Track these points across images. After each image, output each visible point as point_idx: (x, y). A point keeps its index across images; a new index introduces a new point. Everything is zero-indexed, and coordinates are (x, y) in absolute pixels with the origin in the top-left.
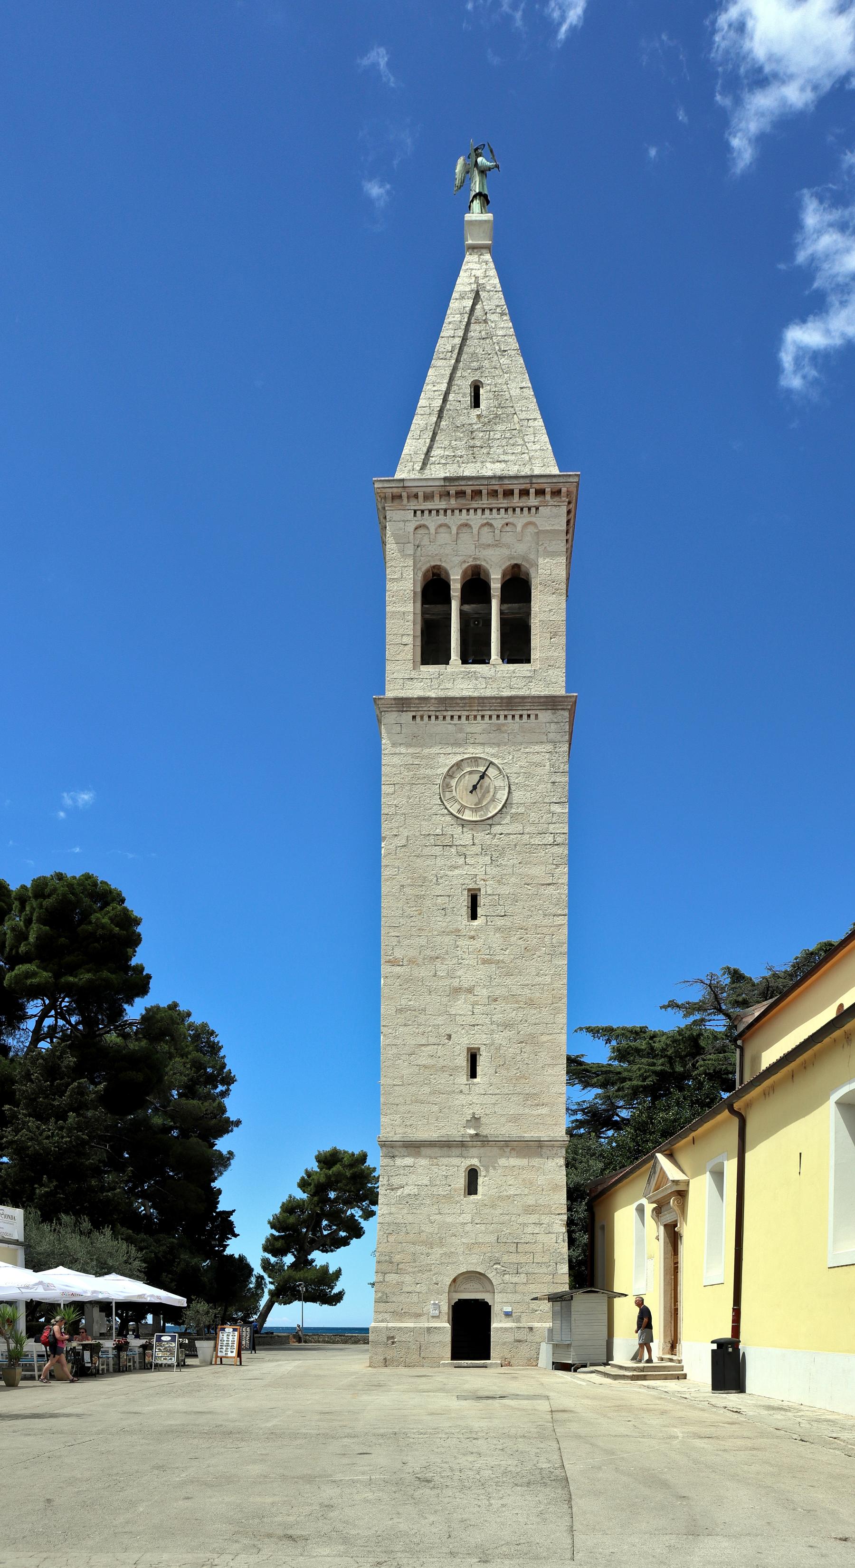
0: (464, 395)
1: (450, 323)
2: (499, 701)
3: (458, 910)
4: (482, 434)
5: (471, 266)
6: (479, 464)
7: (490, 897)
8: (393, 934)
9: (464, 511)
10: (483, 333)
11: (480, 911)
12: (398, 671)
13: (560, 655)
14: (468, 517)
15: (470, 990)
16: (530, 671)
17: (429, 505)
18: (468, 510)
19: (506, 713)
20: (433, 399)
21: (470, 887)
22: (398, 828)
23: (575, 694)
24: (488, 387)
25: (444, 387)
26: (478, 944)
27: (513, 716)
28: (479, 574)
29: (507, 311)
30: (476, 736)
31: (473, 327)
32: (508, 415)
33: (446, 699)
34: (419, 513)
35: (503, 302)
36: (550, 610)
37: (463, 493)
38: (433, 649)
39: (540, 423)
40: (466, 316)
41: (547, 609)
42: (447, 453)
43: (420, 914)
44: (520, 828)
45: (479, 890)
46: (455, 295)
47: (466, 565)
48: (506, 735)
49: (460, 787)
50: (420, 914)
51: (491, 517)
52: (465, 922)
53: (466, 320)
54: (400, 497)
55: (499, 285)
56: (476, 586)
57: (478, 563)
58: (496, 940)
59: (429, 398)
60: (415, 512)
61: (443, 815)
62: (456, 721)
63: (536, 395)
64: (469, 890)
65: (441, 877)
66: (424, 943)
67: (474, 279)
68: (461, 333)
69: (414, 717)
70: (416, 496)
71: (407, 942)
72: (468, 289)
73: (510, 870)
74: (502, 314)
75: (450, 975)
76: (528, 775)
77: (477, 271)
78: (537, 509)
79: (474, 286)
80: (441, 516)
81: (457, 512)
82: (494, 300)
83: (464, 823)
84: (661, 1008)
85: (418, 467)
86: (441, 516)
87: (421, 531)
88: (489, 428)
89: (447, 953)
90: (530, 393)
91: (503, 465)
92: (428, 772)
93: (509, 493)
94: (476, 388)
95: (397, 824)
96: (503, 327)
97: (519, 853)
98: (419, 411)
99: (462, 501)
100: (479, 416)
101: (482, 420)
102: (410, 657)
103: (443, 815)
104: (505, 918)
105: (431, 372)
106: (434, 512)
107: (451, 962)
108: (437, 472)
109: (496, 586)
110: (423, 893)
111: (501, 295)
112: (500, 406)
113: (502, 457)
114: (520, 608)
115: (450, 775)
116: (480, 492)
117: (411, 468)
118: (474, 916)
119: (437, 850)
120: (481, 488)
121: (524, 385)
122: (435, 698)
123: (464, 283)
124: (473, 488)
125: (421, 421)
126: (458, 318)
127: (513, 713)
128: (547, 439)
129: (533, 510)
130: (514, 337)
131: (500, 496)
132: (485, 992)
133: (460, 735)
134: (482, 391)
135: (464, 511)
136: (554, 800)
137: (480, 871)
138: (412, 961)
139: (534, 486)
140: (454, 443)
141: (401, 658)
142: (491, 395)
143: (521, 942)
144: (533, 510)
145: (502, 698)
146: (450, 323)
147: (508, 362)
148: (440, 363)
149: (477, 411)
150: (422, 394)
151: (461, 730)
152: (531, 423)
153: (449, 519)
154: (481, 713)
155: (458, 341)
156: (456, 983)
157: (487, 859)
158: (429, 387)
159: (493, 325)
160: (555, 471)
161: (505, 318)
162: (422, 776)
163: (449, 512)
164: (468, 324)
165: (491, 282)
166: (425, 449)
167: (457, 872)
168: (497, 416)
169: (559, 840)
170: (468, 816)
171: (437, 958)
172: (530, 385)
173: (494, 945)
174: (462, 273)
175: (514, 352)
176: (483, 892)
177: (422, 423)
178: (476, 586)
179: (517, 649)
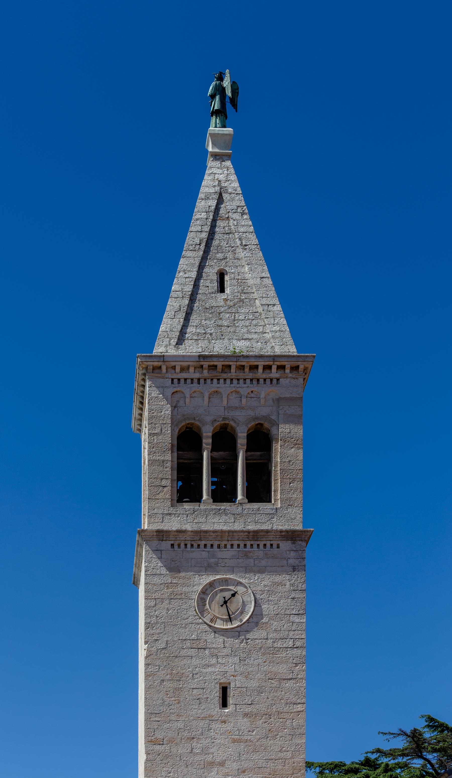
0: (212, 281)
1: (197, 220)
2: (246, 534)
3: (211, 700)
4: (228, 315)
5: (214, 170)
6: (226, 341)
7: (239, 690)
8: (154, 719)
9: (215, 381)
10: (227, 228)
11: (230, 701)
12: (158, 508)
13: (298, 496)
14: (218, 385)
15: (222, 764)
16: (272, 509)
17: (185, 375)
18: (218, 380)
19: (252, 542)
20: (185, 284)
21: (222, 681)
22: (159, 634)
23: (312, 529)
24: (233, 275)
25: (194, 275)
26: (229, 727)
27: (258, 545)
28: (226, 428)
29: (247, 211)
30: (226, 561)
31: (219, 223)
32: (250, 300)
33: (201, 532)
34: (176, 381)
35: (243, 203)
36: (290, 461)
37: (215, 368)
38: (187, 491)
39: (278, 308)
40: (211, 215)
41: (286, 456)
42: (198, 331)
43: (178, 703)
44: (264, 634)
45: (230, 683)
46: (201, 195)
47: (218, 423)
48: (252, 561)
49: (213, 607)
50: (178, 703)
51: (238, 386)
52: (217, 709)
53: (211, 217)
54: (160, 368)
55: (239, 189)
56: (224, 438)
57: (227, 422)
58: (244, 723)
59: (181, 284)
60: (172, 380)
61: (198, 624)
62: (208, 549)
63: (274, 284)
64: (220, 684)
65: (197, 674)
66: (182, 726)
67: (217, 183)
68: (207, 229)
69: (172, 545)
70: (174, 368)
71: (167, 726)
72: (212, 190)
73: (257, 668)
74: (243, 214)
75: (205, 751)
76: (270, 592)
77: (219, 176)
78: (278, 380)
79: (217, 189)
80: (195, 384)
81: (209, 381)
82: (235, 201)
83: (216, 631)
84: (379, 733)
85: (174, 342)
86: (195, 384)
87: (177, 395)
88: (234, 310)
89: (202, 734)
90: (269, 282)
91: (247, 343)
92: (185, 589)
93: (254, 368)
94: (221, 275)
95: (158, 631)
96: (244, 225)
97: (264, 654)
98: (172, 294)
99: (214, 373)
100: (226, 300)
101: (228, 303)
102: (168, 496)
103: (198, 624)
104: (252, 706)
105: (182, 261)
106: (189, 381)
107: (205, 742)
108: (192, 348)
109: (207, 442)
110: (181, 686)
111: (241, 197)
112: (243, 292)
113: (246, 336)
114: (261, 456)
115: (204, 592)
116: (230, 366)
117: (168, 343)
118: (224, 704)
119: (193, 652)
120: (231, 363)
121: (263, 275)
122: (192, 531)
123: (208, 186)
124: (223, 363)
125: (175, 304)
126: (204, 215)
127: (258, 543)
128: (285, 322)
129: (275, 381)
130: (254, 234)
131: (247, 370)
132: (235, 766)
133: (212, 560)
134: (227, 278)
135: (215, 381)
136: (294, 612)
137: (230, 669)
138: (171, 741)
139: (276, 363)
140: (204, 322)
141: (160, 497)
142: (235, 282)
143: (266, 725)
144: (275, 381)
145: (249, 532)
146: (197, 220)
147: (249, 254)
148: (189, 254)
149: (223, 296)
150: (175, 280)
151: (214, 556)
152: (271, 308)
153: (202, 387)
154: (230, 543)
155: (204, 235)
156: (209, 758)
157: (236, 659)
158: (181, 274)
159: (235, 223)
160: (292, 350)
161: (245, 217)
162: (179, 592)
163: (202, 381)
164: (214, 221)
165: (232, 185)
166: (179, 327)
167: (210, 669)
168: (242, 301)
169: (298, 644)
170: (219, 625)
171: (193, 738)
172: (269, 275)
173: (243, 728)
174: (206, 177)
175: (254, 247)
176: (232, 685)
177: (177, 305)
178: (224, 438)
179: (259, 490)
